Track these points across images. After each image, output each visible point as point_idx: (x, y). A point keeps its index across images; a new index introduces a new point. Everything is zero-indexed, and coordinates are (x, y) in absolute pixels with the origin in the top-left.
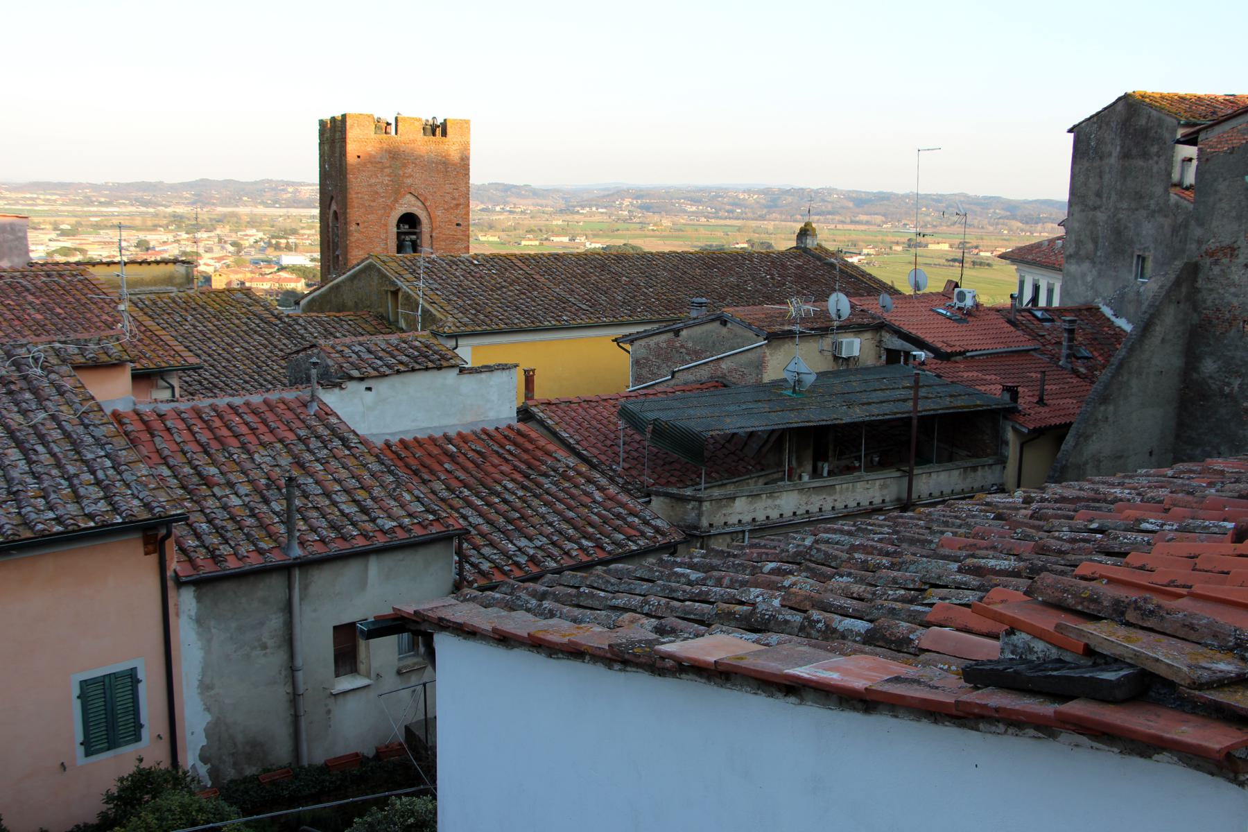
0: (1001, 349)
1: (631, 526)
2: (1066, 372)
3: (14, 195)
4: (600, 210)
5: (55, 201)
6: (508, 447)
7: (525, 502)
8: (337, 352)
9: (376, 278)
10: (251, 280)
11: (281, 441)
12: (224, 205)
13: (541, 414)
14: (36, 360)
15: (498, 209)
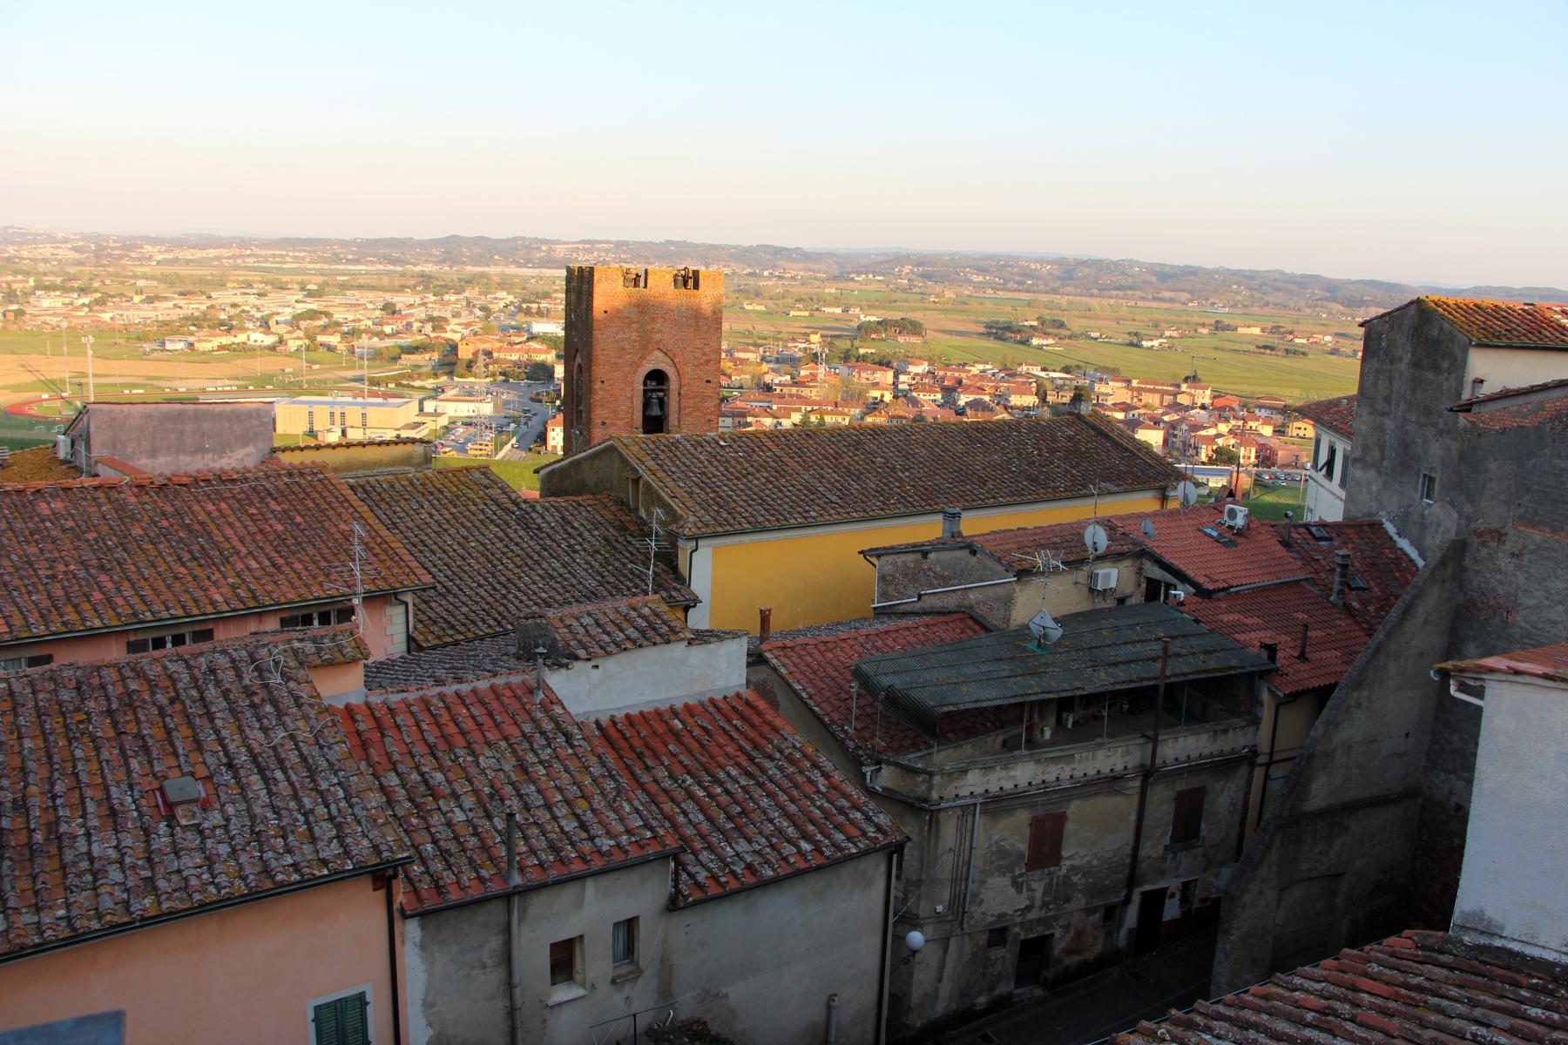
0: (1269, 581)
1: (852, 822)
2: (1335, 610)
3: (263, 253)
5: (303, 258)
6: (734, 722)
7: (747, 792)
8: (566, 626)
10: (500, 350)
11: (506, 739)
12: (476, 264)
13: (774, 661)
14: (277, 663)
15: (766, 273)
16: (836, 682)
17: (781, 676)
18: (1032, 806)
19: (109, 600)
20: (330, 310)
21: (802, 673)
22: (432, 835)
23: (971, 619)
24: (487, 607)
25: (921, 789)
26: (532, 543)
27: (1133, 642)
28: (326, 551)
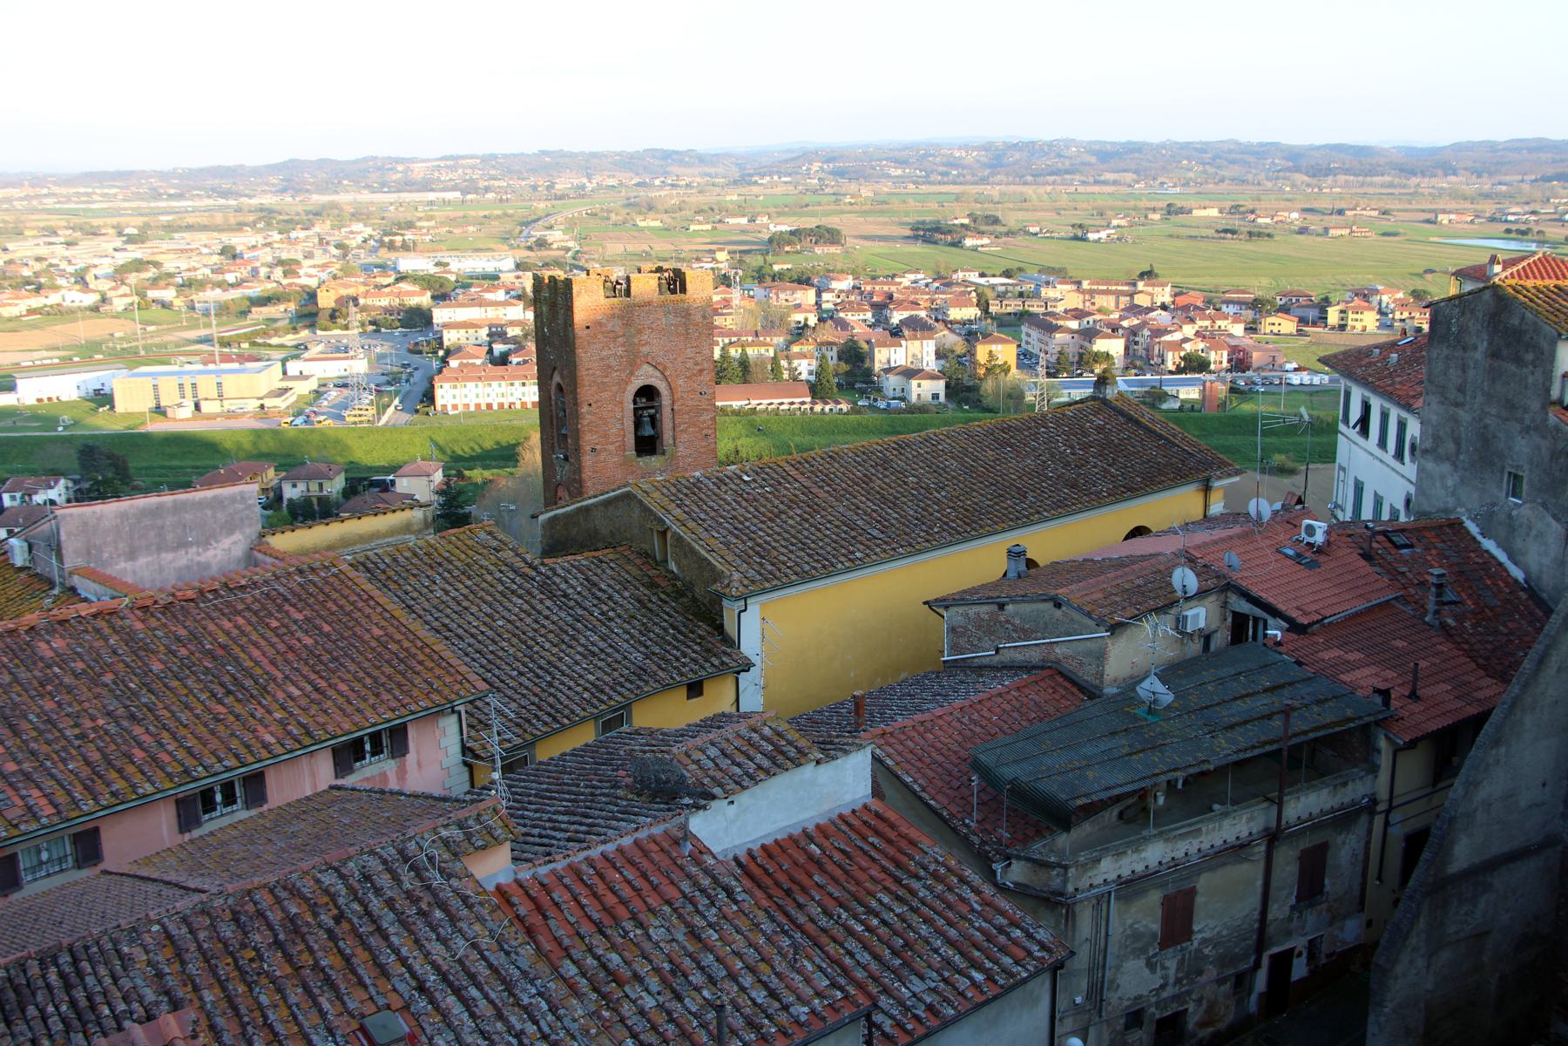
0: (1361, 605)
1: (1015, 942)
2: (1433, 632)
3: (64, 191)
4: (784, 179)
6: (871, 840)
7: (904, 921)
8: (694, 762)
9: (636, 513)
10: (366, 295)
12: (321, 191)
15: (657, 182)
16: (944, 768)
18: (1163, 886)
19: (154, 759)
20: (158, 258)
21: (908, 762)
22: (629, 1028)
23: (1056, 673)
24: (536, 700)
25: (1056, 883)
26: (563, 615)
27: (1242, 697)
28: (367, 664)
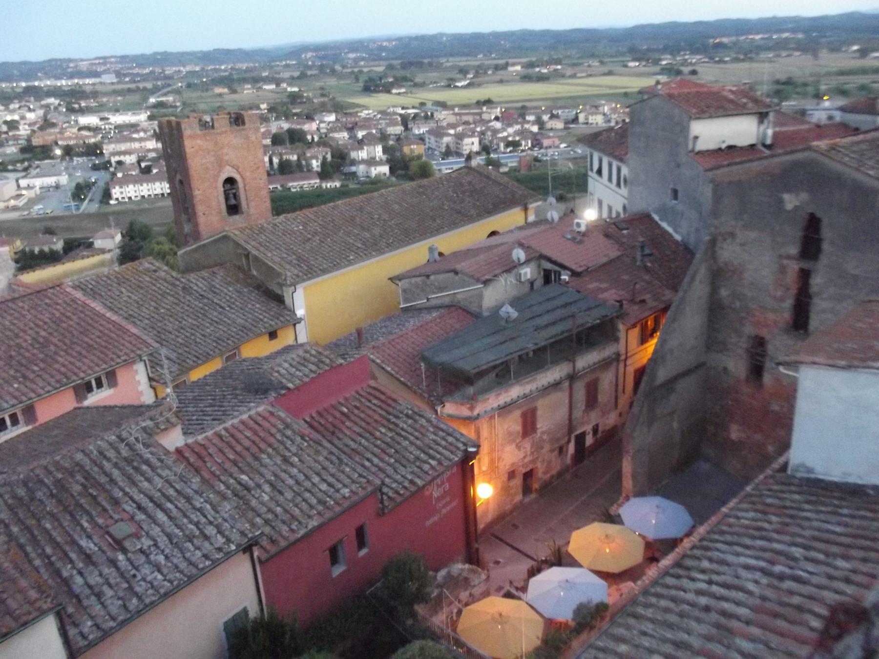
17: (377, 364)
